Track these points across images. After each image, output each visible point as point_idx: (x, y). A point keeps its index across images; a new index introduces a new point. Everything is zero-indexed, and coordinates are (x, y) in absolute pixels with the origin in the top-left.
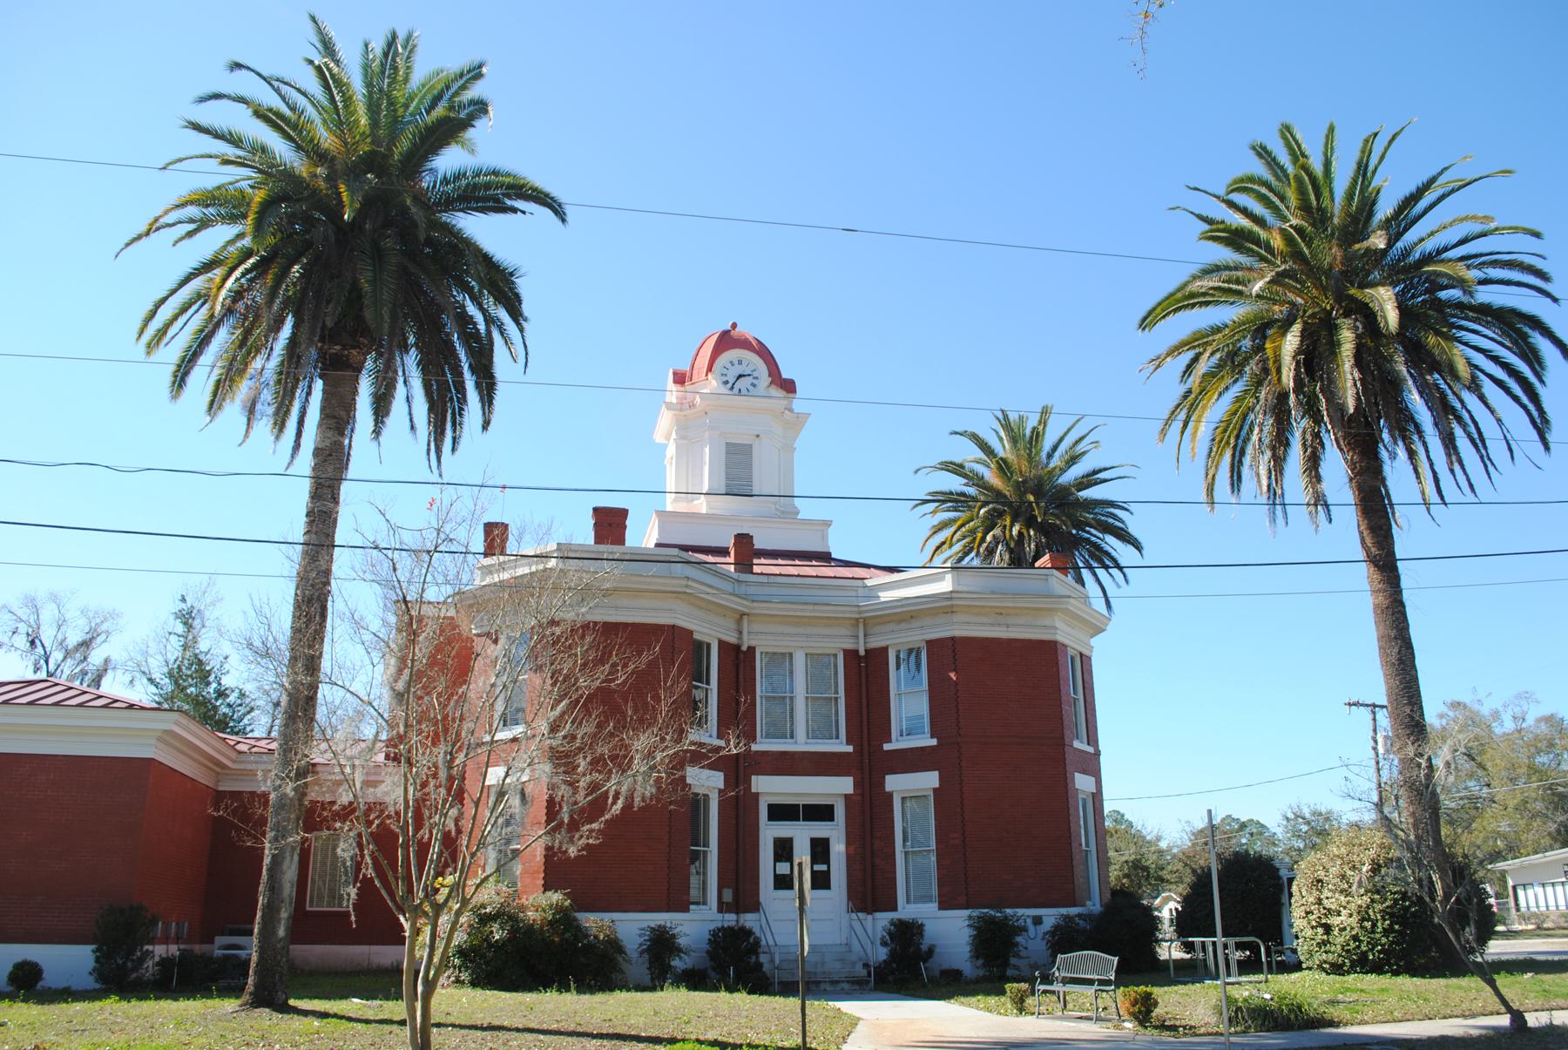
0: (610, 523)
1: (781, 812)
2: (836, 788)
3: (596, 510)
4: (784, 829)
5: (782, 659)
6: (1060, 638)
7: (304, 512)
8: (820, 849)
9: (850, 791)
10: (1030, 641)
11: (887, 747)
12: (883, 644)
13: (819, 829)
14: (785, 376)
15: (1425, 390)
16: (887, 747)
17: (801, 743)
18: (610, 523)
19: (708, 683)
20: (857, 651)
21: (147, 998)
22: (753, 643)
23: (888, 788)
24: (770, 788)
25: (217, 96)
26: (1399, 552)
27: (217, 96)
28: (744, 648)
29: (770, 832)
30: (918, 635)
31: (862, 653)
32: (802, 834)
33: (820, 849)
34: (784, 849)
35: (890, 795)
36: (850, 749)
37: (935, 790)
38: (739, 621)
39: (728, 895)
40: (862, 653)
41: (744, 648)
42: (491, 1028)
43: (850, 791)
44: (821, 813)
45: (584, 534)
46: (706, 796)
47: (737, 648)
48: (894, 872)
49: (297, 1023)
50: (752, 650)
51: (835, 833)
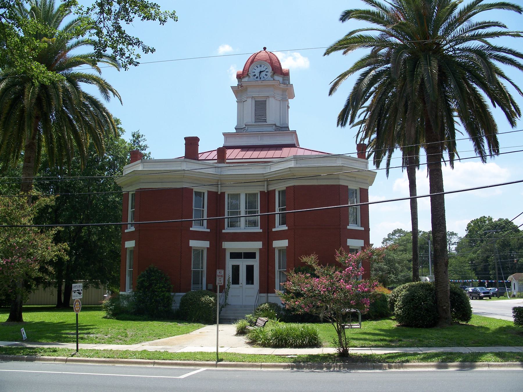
0: (192, 143)
1: (235, 255)
2: (256, 246)
3: (185, 138)
4: (236, 262)
5: (237, 196)
8: (250, 269)
10: (327, 185)
11: (274, 230)
12: (274, 188)
13: (249, 262)
15: (437, 355)
16: (274, 230)
17: (242, 228)
18: (192, 143)
19: (203, 208)
21: (489, 113)
22: (223, 191)
24: (230, 246)
25: (336, 84)
26: (446, 188)
27: (336, 84)
28: (219, 193)
29: (230, 263)
30: (282, 186)
32: (243, 264)
33: (250, 269)
34: (236, 269)
36: (261, 231)
40: (266, 191)
41: (219, 193)
44: (251, 255)
45: (181, 152)
50: (223, 194)
51: (255, 263)
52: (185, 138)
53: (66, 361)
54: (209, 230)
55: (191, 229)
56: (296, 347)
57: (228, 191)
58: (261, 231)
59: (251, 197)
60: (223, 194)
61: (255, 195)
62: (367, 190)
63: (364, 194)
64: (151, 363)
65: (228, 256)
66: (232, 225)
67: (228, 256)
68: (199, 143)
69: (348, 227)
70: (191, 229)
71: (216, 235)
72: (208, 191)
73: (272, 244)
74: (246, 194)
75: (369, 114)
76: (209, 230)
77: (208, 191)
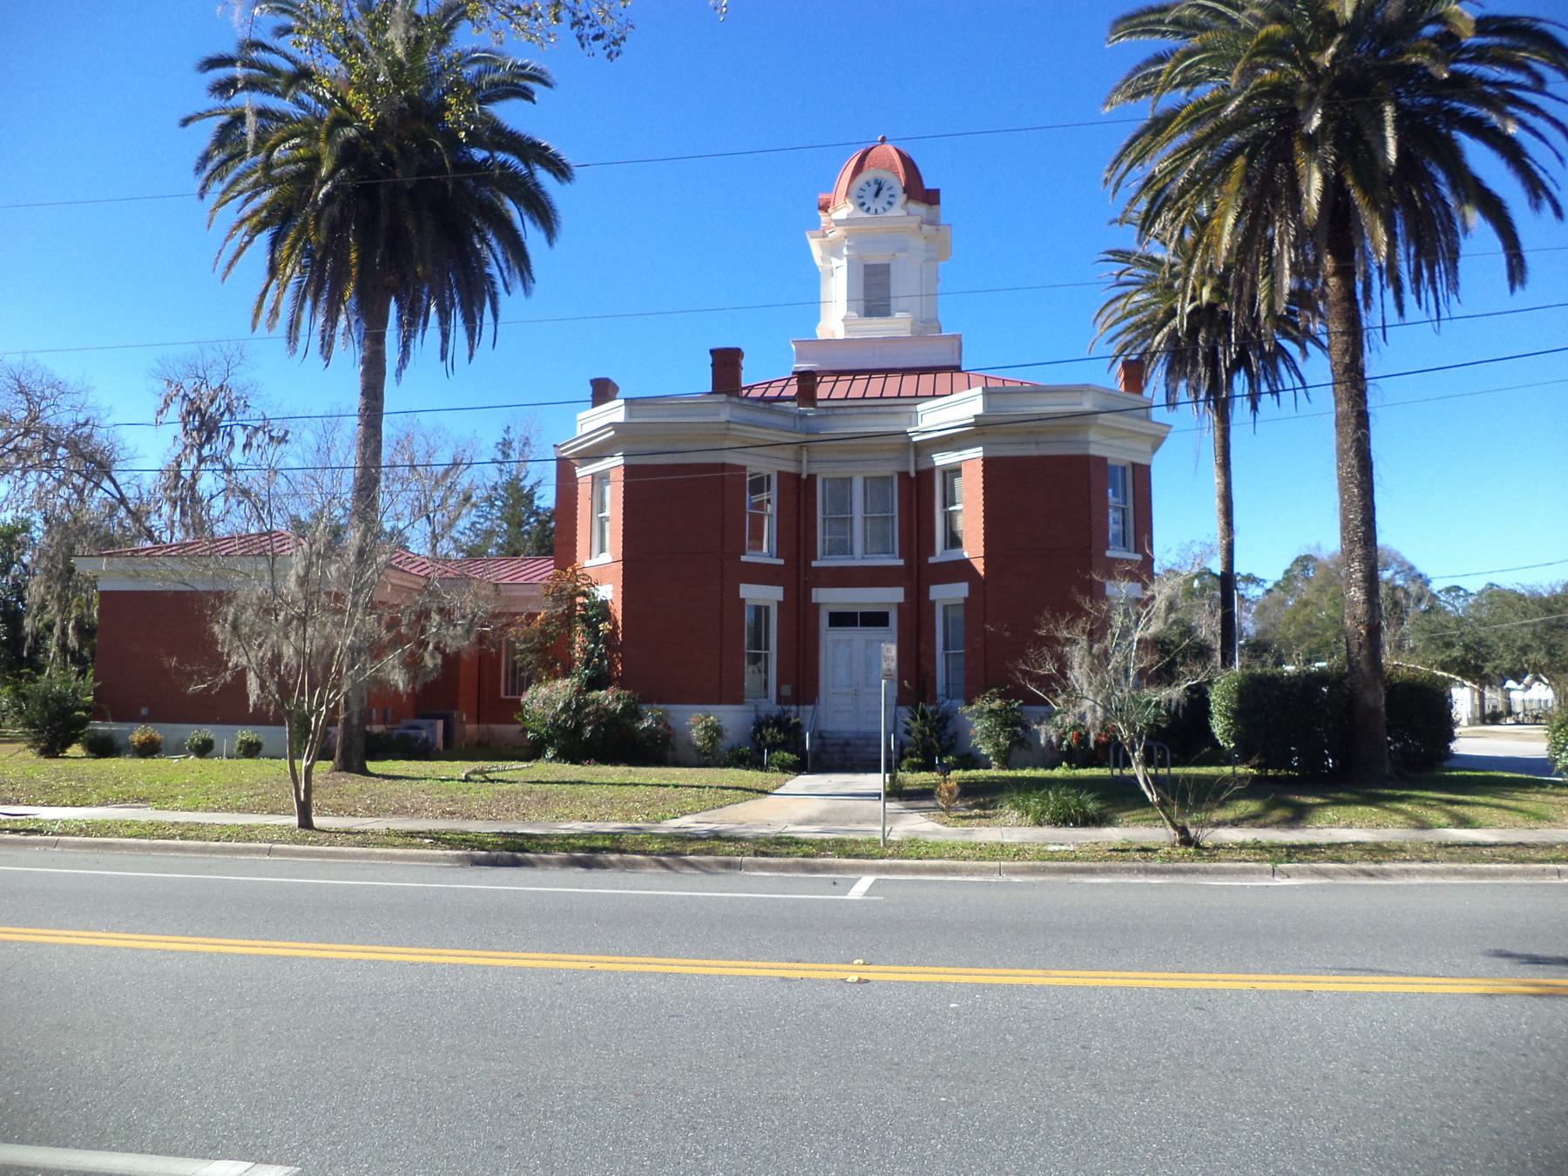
0: (726, 364)
1: (841, 619)
2: (890, 597)
3: (712, 352)
6: (1094, 450)
7: (359, 391)
9: (902, 599)
14: (928, 185)
17: (858, 559)
18: (726, 364)
20: (907, 474)
22: (812, 472)
23: (932, 597)
24: (829, 598)
26: (387, 406)
28: (804, 476)
31: (913, 474)
35: (817, 606)
36: (901, 562)
37: (899, 605)
38: (798, 453)
39: (787, 690)
40: (913, 474)
41: (804, 476)
42: (580, 782)
43: (902, 599)
44: (876, 619)
45: (703, 380)
46: (767, 608)
47: (797, 476)
48: (934, 671)
49: (369, 783)
50: (812, 478)
52: (712, 352)
53: (270, 852)
54: (781, 562)
55: (743, 558)
56: (239, 810)
57: (823, 472)
58: (901, 562)
59: (875, 485)
60: (812, 478)
61: (886, 480)
62: (1148, 467)
63: (1142, 475)
64: (1552, 873)
65: (824, 620)
66: (555, 538)
67: (824, 620)
68: (744, 363)
69: (1109, 554)
70: (743, 558)
71: (798, 573)
72: (780, 473)
73: (906, 594)
74: (865, 479)
75: (494, 243)
76: (781, 562)
77: (780, 473)
